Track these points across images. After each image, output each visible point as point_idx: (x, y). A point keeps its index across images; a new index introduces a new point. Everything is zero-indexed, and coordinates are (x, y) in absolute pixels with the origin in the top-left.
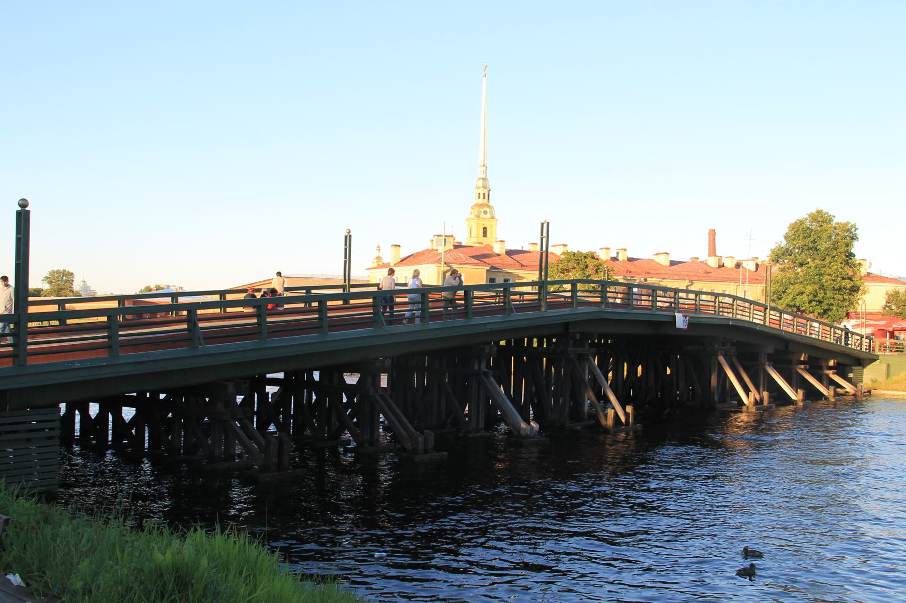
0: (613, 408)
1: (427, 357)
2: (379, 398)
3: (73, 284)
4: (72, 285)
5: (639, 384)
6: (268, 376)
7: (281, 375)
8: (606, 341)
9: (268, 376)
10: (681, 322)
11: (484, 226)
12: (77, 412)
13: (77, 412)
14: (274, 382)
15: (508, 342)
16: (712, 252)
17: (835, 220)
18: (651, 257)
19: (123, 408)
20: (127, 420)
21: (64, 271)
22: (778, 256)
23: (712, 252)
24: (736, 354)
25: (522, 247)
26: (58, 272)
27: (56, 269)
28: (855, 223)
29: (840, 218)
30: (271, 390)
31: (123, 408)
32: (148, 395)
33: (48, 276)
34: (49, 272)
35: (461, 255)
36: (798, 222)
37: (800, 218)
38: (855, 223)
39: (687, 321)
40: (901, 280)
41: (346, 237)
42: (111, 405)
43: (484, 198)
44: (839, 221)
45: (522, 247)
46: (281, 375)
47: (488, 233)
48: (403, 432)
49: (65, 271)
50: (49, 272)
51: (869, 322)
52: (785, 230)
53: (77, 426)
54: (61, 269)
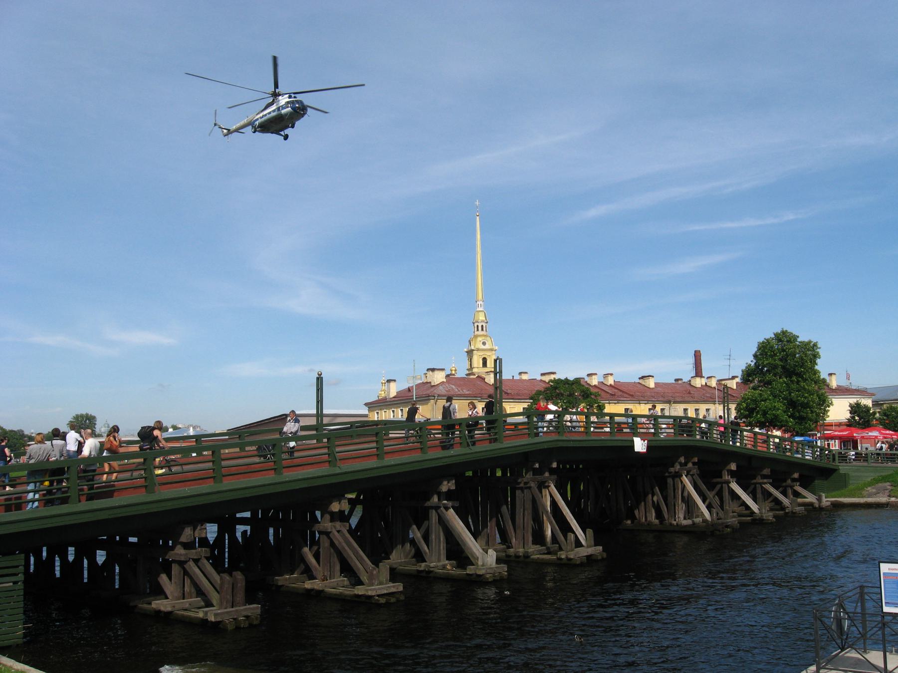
0: (573, 532)
1: (260, 517)
2: (336, 533)
3: (96, 426)
4: (95, 428)
5: (357, 579)
6: (238, 515)
7: (247, 514)
8: (578, 466)
9: (238, 515)
10: (640, 445)
11: (483, 357)
12: (57, 559)
13: (57, 559)
14: (243, 521)
15: (475, 473)
16: (699, 373)
17: (799, 340)
18: (638, 381)
19: (98, 551)
20: (212, 539)
21: (87, 415)
22: (748, 375)
23: (699, 373)
24: (698, 472)
25: (513, 376)
26: (82, 416)
27: (79, 414)
28: (817, 342)
29: (803, 338)
30: (240, 528)
31: (98, 551)
32: (118, 538)
33: (468, 372)
34: (74, 417)
35: (454, 387)
36: (765, 341)
37: (768, 337)
38: (817, 342)
39: (646, 445)
40: (869, 391)
41: (318, 379)
42: (86, 550)
43: (482, 330)
44: (803, 340)
45: (513, 376)
46: (247, 514)
47: (481, 362)
48: (360, 566)
49: (88, 414)
50: (74, 417)
51: (834, 433)
52: (754, 349)
53: (58, 569)
54: (84, 413)
